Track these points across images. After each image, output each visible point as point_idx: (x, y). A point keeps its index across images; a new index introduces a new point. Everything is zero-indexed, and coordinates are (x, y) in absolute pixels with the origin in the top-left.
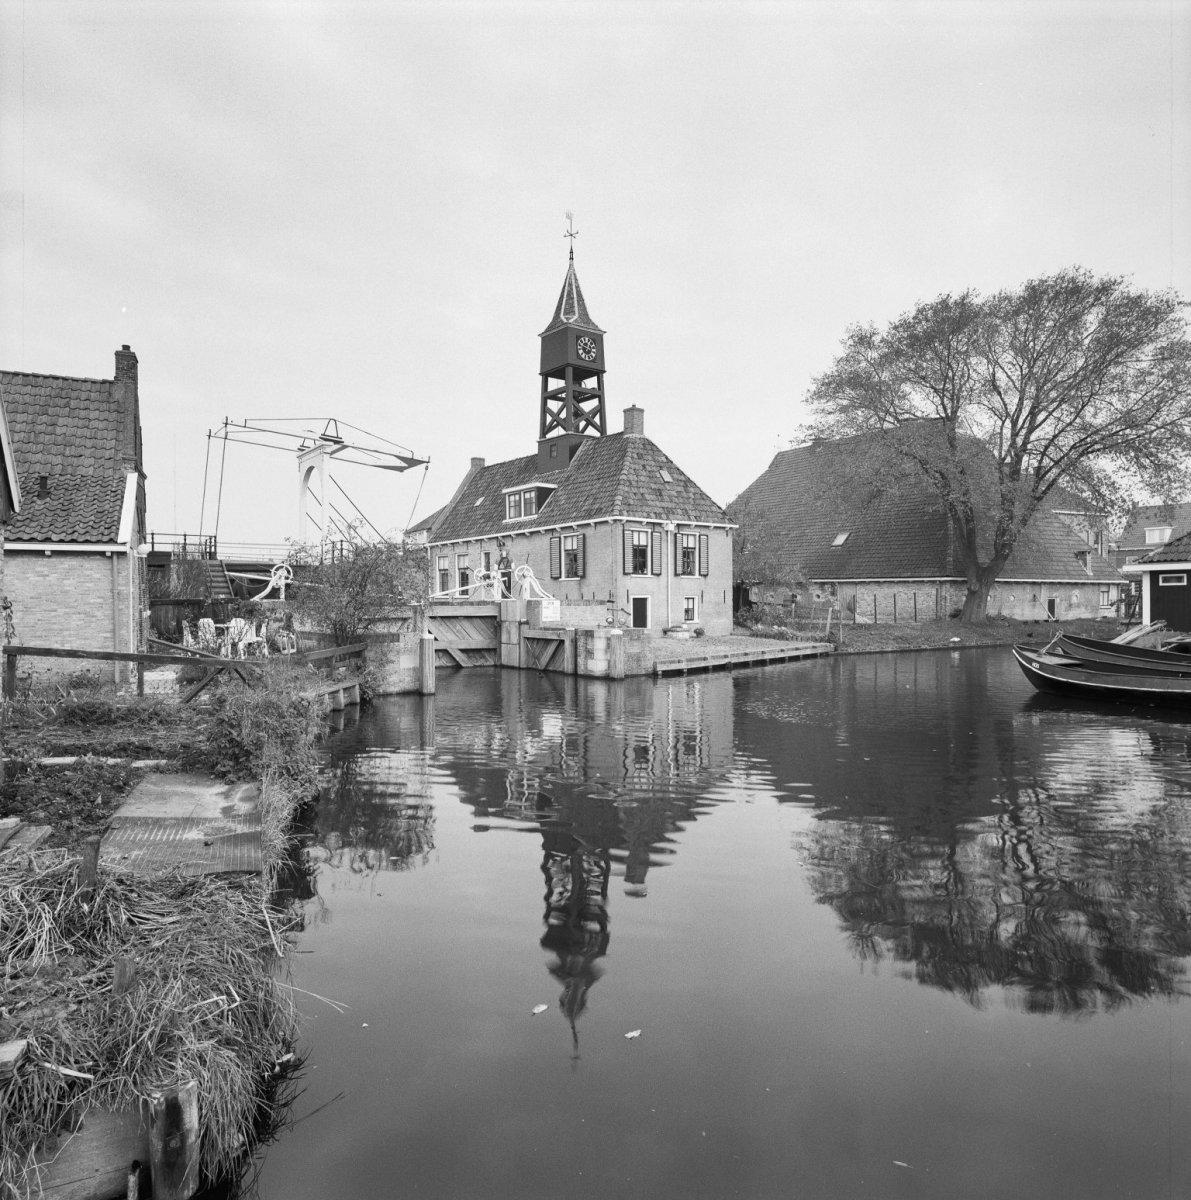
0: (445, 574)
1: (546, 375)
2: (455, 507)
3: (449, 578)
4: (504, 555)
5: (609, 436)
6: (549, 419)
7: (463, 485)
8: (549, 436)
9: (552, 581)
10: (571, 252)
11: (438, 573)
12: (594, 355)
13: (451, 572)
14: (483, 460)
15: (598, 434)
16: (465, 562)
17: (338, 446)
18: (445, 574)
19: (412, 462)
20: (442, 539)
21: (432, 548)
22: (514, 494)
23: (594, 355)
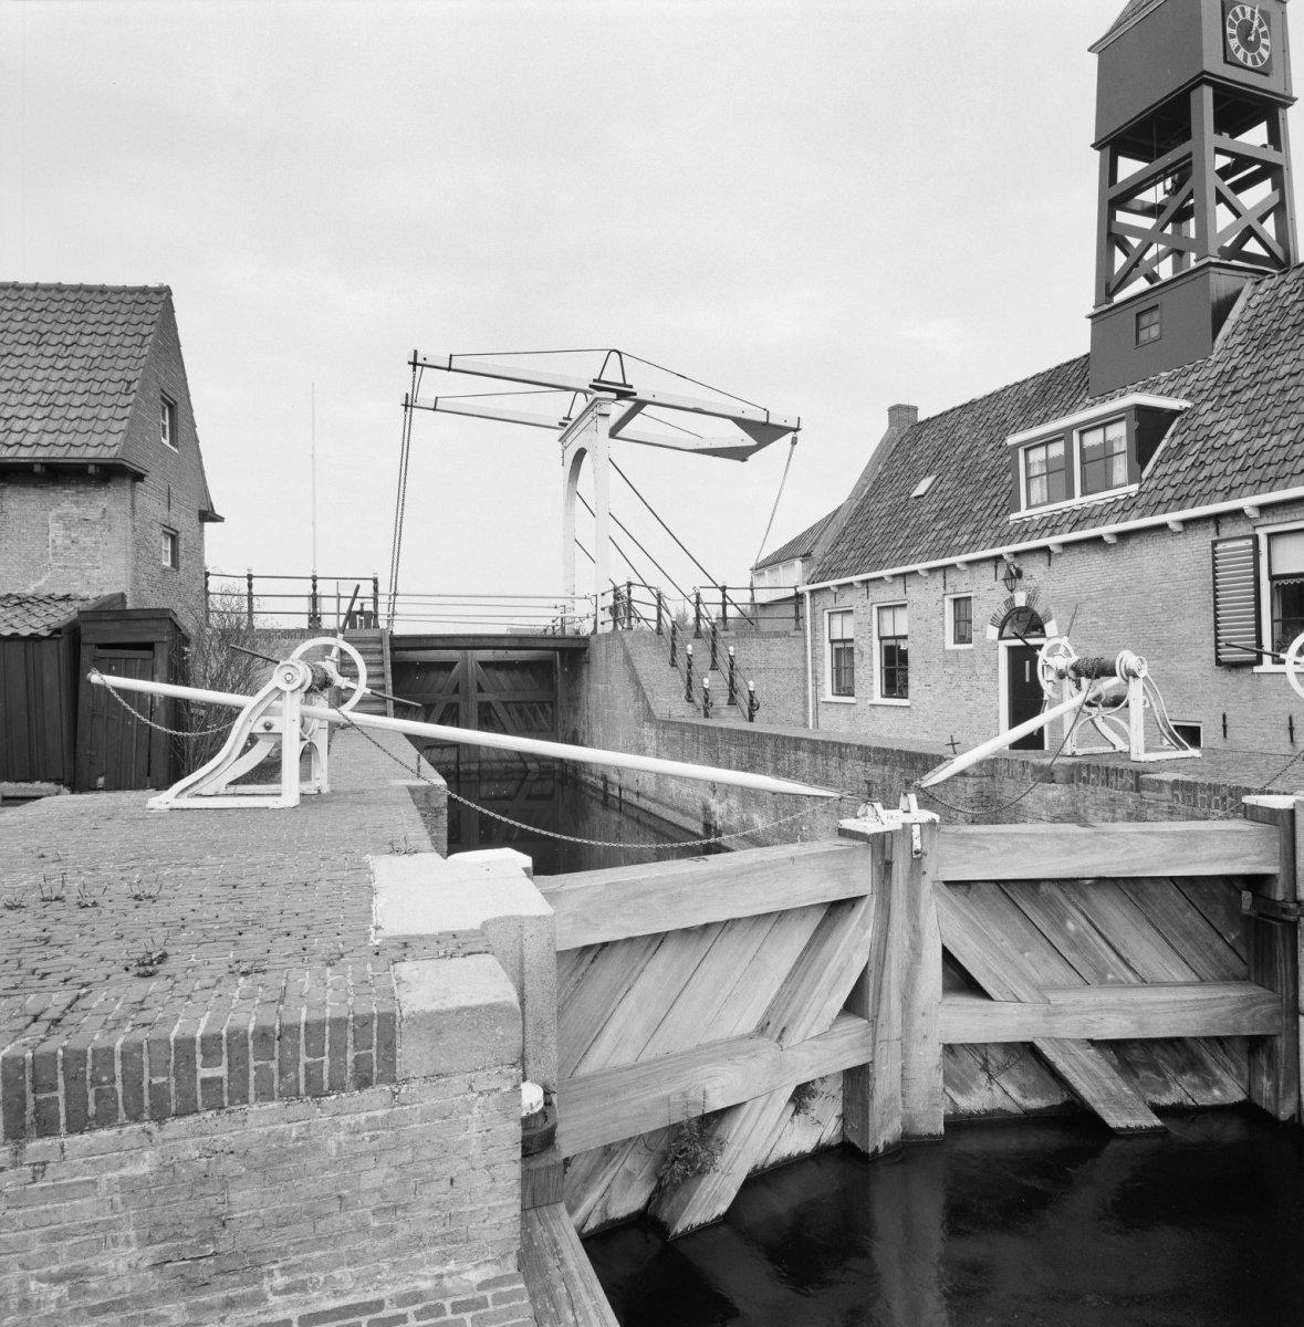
0: (844, 652)
3: (857, 659)
4: (1020, 600)
7: (875, 460)
9: (1222, 676)
11: (828, 646)
12: (1266, 54)
13: (860, 645)
14: (915, 409)
16: (899, 624)
17: (627, 405)
18: (844, 652)
19: (765, 432)
20: (839, 573)
21: (813, 592)
22: (1046, 441)
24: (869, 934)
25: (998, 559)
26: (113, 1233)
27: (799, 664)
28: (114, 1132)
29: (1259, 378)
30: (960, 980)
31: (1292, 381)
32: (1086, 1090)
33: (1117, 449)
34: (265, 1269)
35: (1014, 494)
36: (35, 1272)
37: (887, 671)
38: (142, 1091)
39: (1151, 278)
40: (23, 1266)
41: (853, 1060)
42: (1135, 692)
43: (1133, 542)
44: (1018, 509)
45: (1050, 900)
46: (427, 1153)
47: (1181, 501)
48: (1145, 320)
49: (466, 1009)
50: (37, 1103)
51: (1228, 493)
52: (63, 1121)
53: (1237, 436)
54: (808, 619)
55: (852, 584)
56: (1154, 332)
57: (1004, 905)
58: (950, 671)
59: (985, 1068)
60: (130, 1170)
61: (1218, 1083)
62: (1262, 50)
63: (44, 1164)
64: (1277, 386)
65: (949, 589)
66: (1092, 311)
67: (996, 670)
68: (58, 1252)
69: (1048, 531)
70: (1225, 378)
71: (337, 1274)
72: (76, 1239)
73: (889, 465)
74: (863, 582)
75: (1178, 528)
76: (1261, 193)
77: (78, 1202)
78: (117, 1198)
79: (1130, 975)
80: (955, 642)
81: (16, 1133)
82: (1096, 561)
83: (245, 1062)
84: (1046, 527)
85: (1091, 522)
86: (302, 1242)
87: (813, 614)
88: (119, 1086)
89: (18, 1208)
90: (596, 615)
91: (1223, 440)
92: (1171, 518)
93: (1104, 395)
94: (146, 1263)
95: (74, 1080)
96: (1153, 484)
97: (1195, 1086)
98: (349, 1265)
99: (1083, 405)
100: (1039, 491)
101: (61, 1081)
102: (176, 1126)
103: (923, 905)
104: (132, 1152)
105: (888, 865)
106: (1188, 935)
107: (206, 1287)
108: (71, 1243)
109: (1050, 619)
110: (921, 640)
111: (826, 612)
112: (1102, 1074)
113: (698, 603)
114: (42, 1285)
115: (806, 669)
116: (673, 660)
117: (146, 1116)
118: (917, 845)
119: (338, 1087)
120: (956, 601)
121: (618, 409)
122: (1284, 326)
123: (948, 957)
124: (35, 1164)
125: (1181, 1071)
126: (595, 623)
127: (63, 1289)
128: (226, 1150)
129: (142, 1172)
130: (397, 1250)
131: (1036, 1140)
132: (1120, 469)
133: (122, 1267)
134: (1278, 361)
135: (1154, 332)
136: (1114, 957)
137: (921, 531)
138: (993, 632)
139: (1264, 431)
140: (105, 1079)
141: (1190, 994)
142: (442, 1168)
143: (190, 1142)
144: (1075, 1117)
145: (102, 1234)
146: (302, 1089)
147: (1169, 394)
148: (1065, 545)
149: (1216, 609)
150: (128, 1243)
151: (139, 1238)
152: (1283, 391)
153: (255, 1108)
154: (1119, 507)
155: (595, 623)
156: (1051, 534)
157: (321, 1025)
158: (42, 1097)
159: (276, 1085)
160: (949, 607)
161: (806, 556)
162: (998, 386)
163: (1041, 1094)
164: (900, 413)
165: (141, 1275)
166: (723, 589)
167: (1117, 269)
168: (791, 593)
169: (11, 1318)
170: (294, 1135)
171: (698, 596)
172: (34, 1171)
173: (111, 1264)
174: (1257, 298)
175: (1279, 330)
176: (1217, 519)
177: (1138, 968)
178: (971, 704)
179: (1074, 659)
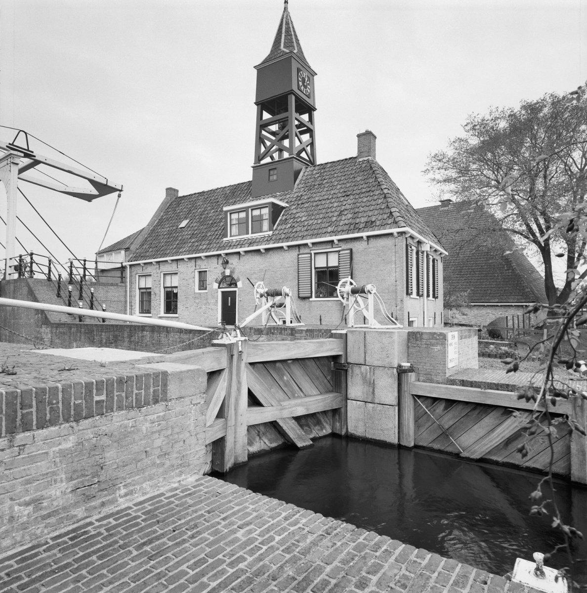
2: (153, 231)
3: (152, 297)
4: (228, 272)
5: (323, 166)
6: (263, 149)
7: (160, 209)
8: (263, 162)
11: (138, 291)
19: (104, 189)
20: (145, 257)
21: (131, 266)
24: (226, 384)
25: (219, 255)
26: (55, 477)
27: (123, 299)
28: (57, 428)
29: (309, 200)
30: (254, 401)
31: (320, 203)
32: (292, 435)
33: (265, 217)
34: (117, 487)
35: (225, 229)
36: (18, 501)
37: (167, 302)
38: (71, 407)
39: (272, 158)
40: (11, 499)
41: (219, 436)
42: (288, 301)
43: (271, 252)
44: (226, 236)
45: (279, 369)
46: (176, 430)
47: (287, 239)
48: (272, 172)
49: (190, 370)
50: (23, 415)
51: (303, 238)
52: (35, 423)
53: (304, 219)
54: (128, 278)
55: (152, 263)
56: (275, 177)
57: (265, 372)
58: (197, 301)
59: (259, 435)
60: (64, 446)
61: (325, 427)
63: (24, 445)
64: (315, 204)
65: (197, 267)
66: (253, 165)
67: (217, 301)
68: (29, 490)
69: (239, 246)
70: (299, 198)
71: (144, 485)
72: (38, 482)
73: (167, 212)
74: (157, 262)
75: (286, 248)
76: (306, 137)
77: (39, 464)
78: (58, 460)
79: (302, 394)
80: (199, 290)
81: (12, 431)
82: (257, 259)
83: (113, 393)
84: (238, 245)
85: (256, 244)
86: (131, 473)
87: (131, 276)
88: (60, 405)
89: (10, 469)
90: (5, 270)
91: (300, 219)
92: (284, 244)
93: (258, 197)
94: (69, 490)
95: (40, 402)
96: (277, 232)
97: (319, 430)
98: (148, 481)
99: (249, 200)
100: (235, 230)
101: (34, 403)
102: (85, 423)
103: (242, 373)
104: (65, 437)
105: (232, 356)
106: (318, 378)
107: (93, 499)
108: (35, 484)
109: (239, 281)
110: (184, 288)
111: (137, 275)
112: (296, 429)
113: (71, 267)
114: (21, 508)
115: (126, 302)
116: (59, 294)
117: (72, 419)
118: (240, 349)
119: (147, 404)
120: (200, 272)
121: (27, 161)
122: (316, 184)
123: (250, 394)
124: (20, 446)
125: (315, 426)
126: (5, 274)
127: (31, 508)
128: (104, 433)
129: (69, 446)
130: (166, 472)
131: (275, 457)
132: (266, 225)
133: (58, 493)
134: (315, 195)
135: (275, 177)
136: (297, 388)
137: (184, 242)
138: (216, 285)
139: (312, 218)
140: (54, 402)
141: (320, 397)
142: (181, 436)
143: (89, 431)
144: (289, 447)
145: (50, 478)
146: (134, 405)
147: (281, 200)
148: (246, 252)
149: (299, 278)
150: (62, 481)
151: (66, 478)
152: (317, 206)
153: (116, 414)
154: (266, 239)
155: (5, 274)
156: (241, 247)
157: (141, 376)
158: (25, 411)
159: (124, 403)
161: (127, 249)
162: (214, 187)
163: (275, 441)
164: (171, 191)
165: (66, 496)
168: (120, 265)
169: (4, 527)
170: (130, 425)
171: (71, 263)
172: (20, 449)
173: (53, 492)
174: (306, 173)
175: (314, 185)
176: (299, 246)
177: (304, 391)
178: (206, 315)
179: (266, 290)
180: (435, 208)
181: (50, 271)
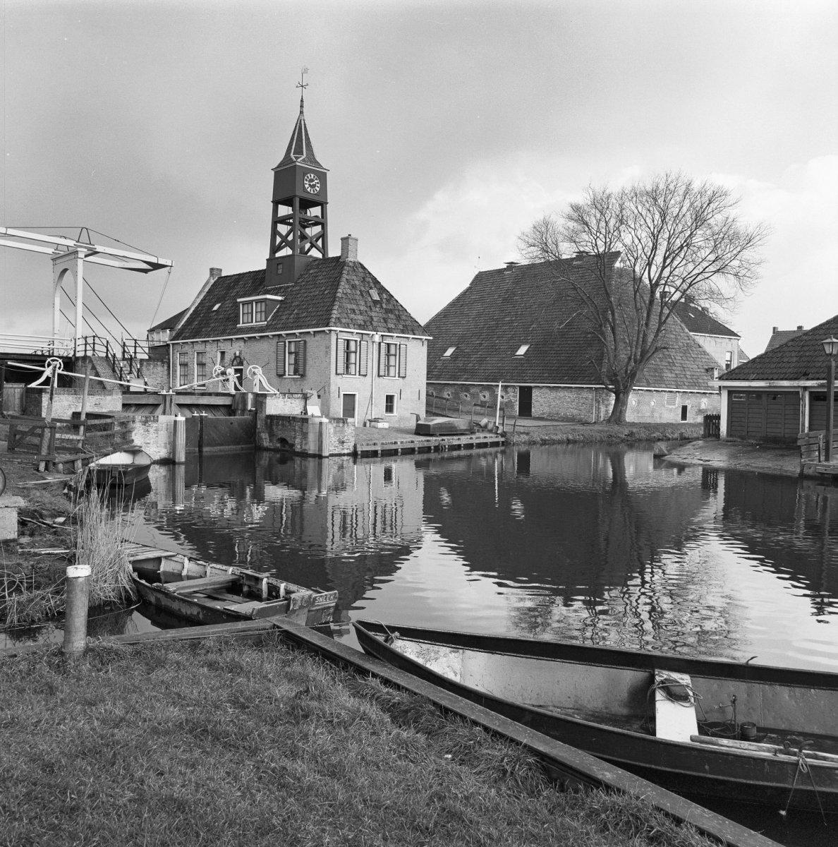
1: (276, 203)
6: (278, 240)
8: (278, 255)
10: (302, 101)
12: (318, 189)
15: (320, 256)
19: (156, 266)
21: (173, 344)
23: (318, 189)
62: (316, 188)
160: (219, 355)
166: (135, 340)
167: (277, 243)
180: (500, 271)
181: (108, 350)
